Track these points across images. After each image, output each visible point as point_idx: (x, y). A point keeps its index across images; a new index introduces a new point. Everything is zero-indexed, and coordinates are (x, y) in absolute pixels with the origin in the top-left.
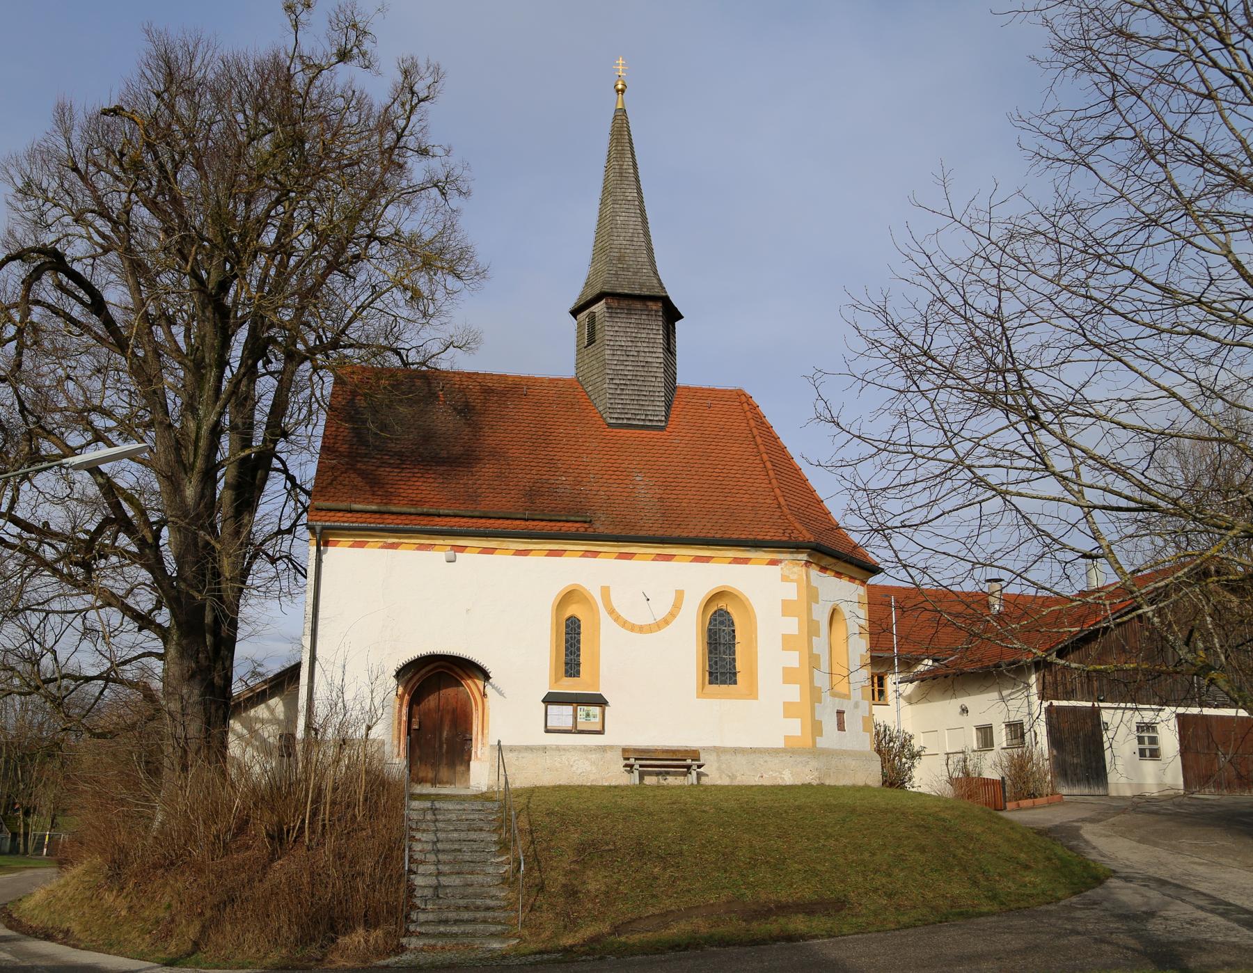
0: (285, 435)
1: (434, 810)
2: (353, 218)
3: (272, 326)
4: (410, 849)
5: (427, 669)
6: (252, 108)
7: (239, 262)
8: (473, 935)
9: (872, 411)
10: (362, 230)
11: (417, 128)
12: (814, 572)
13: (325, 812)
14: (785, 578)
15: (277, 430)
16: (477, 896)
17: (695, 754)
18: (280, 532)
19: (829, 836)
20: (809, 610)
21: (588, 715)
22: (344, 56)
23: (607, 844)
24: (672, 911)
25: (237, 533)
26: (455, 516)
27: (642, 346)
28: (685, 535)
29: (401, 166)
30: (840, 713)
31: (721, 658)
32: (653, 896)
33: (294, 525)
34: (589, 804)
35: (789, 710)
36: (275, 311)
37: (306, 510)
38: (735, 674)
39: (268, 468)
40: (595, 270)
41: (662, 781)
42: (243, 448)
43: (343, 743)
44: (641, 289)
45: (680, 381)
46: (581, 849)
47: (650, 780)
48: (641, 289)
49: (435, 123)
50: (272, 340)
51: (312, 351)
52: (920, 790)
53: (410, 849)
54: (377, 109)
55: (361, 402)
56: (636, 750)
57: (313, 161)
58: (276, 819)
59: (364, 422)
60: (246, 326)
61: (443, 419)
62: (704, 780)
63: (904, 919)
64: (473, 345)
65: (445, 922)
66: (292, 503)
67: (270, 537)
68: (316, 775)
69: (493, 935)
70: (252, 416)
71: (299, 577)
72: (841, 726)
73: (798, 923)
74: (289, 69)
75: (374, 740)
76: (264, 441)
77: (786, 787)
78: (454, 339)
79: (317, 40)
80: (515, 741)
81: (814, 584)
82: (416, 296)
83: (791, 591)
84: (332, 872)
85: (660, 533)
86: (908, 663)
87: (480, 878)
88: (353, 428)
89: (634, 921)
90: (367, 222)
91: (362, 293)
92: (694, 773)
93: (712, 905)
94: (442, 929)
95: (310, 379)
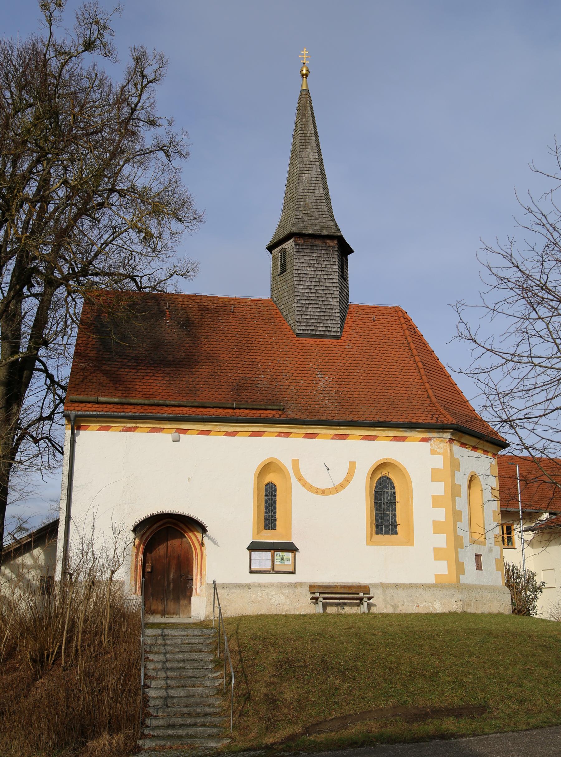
0: (46, 344)
1: (164, 636)
2: (98, 175)
3: (35, 258)
4: (145, 668)
5: (158, 524)
6: (17, 87)
7: (9, 210)
8: (195, 736)
9: (501, 328)
10: (105, 184)
11: (147, 104)
12: (456, 447)
13: (78, 639)
14: (433, 452)
15: (39, 339)
16: (198, 704)
17: (365, 589)
18: (41, 419)
19: (472, 654)
20: (453, 476)
21: (283, 559)
22: (89, 46)
23: (299, 661)
24: (350, 715)
25: (7, 420)
26: (179, 406)
27: (323, 275)
28: (356, 419)
29: (134, 133)
30: (478, 556)
31: (385, 515)
32: (336, 703)
33: (53, 413)
34: (285, 629)
35: (438, 554)
36: (37, 247)
37: (62, 401)
38: (396, 526)
39: (33, 369)
40: (286, 215)
41: (340, 611)
42: (12, 354)
43: (93, 584)
44: (321, 230)
45: (352, 300)
46: (278, 665)
47: (331, 610)
48: (321, 230)
49: (160, 100)
50: (35, 270)
51: (66, 279)
52: (542, 617)
53: (145, 668)
54: (116, 89)
55: (105, 319)
56: (320, 586)
57: (65, 131)
58: (38, 646)
59: (108, 333)
60: (14, 258)
61: (169, 330)
62: (373, 610)
63: (533, 721)
64: (191, 273)
65: (173, 726)
66: (51, 396)
67: (34, 423)
68: (71, 610)
69: (210, 736)
70: (19, 329)
71: (57, 453)
72: (479, 566)
73: (450, 724)
74: (45, 55)
75: (117, 581)
76: (29, 348)
77: (437, 614)
78: (178, 268)
79: (67, 33)
80: (227, 578)
81: (456, 456)
82: (148, 236)
83: (438, 462)
84: (83, 688)
85: (337, 418)
86: (529, 516)
87: (200, 690)
88: (100, 339)
89: (320, 723)
90: (109, 178)
91: (105, 232)
92: (365, 604)
93: (382, 710)
94: (170, 732)
95: (66, 301)
